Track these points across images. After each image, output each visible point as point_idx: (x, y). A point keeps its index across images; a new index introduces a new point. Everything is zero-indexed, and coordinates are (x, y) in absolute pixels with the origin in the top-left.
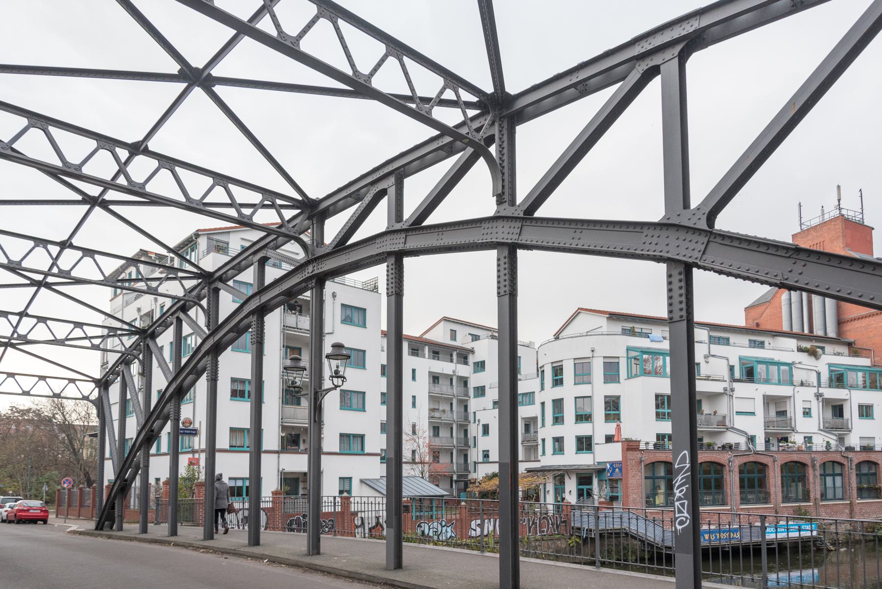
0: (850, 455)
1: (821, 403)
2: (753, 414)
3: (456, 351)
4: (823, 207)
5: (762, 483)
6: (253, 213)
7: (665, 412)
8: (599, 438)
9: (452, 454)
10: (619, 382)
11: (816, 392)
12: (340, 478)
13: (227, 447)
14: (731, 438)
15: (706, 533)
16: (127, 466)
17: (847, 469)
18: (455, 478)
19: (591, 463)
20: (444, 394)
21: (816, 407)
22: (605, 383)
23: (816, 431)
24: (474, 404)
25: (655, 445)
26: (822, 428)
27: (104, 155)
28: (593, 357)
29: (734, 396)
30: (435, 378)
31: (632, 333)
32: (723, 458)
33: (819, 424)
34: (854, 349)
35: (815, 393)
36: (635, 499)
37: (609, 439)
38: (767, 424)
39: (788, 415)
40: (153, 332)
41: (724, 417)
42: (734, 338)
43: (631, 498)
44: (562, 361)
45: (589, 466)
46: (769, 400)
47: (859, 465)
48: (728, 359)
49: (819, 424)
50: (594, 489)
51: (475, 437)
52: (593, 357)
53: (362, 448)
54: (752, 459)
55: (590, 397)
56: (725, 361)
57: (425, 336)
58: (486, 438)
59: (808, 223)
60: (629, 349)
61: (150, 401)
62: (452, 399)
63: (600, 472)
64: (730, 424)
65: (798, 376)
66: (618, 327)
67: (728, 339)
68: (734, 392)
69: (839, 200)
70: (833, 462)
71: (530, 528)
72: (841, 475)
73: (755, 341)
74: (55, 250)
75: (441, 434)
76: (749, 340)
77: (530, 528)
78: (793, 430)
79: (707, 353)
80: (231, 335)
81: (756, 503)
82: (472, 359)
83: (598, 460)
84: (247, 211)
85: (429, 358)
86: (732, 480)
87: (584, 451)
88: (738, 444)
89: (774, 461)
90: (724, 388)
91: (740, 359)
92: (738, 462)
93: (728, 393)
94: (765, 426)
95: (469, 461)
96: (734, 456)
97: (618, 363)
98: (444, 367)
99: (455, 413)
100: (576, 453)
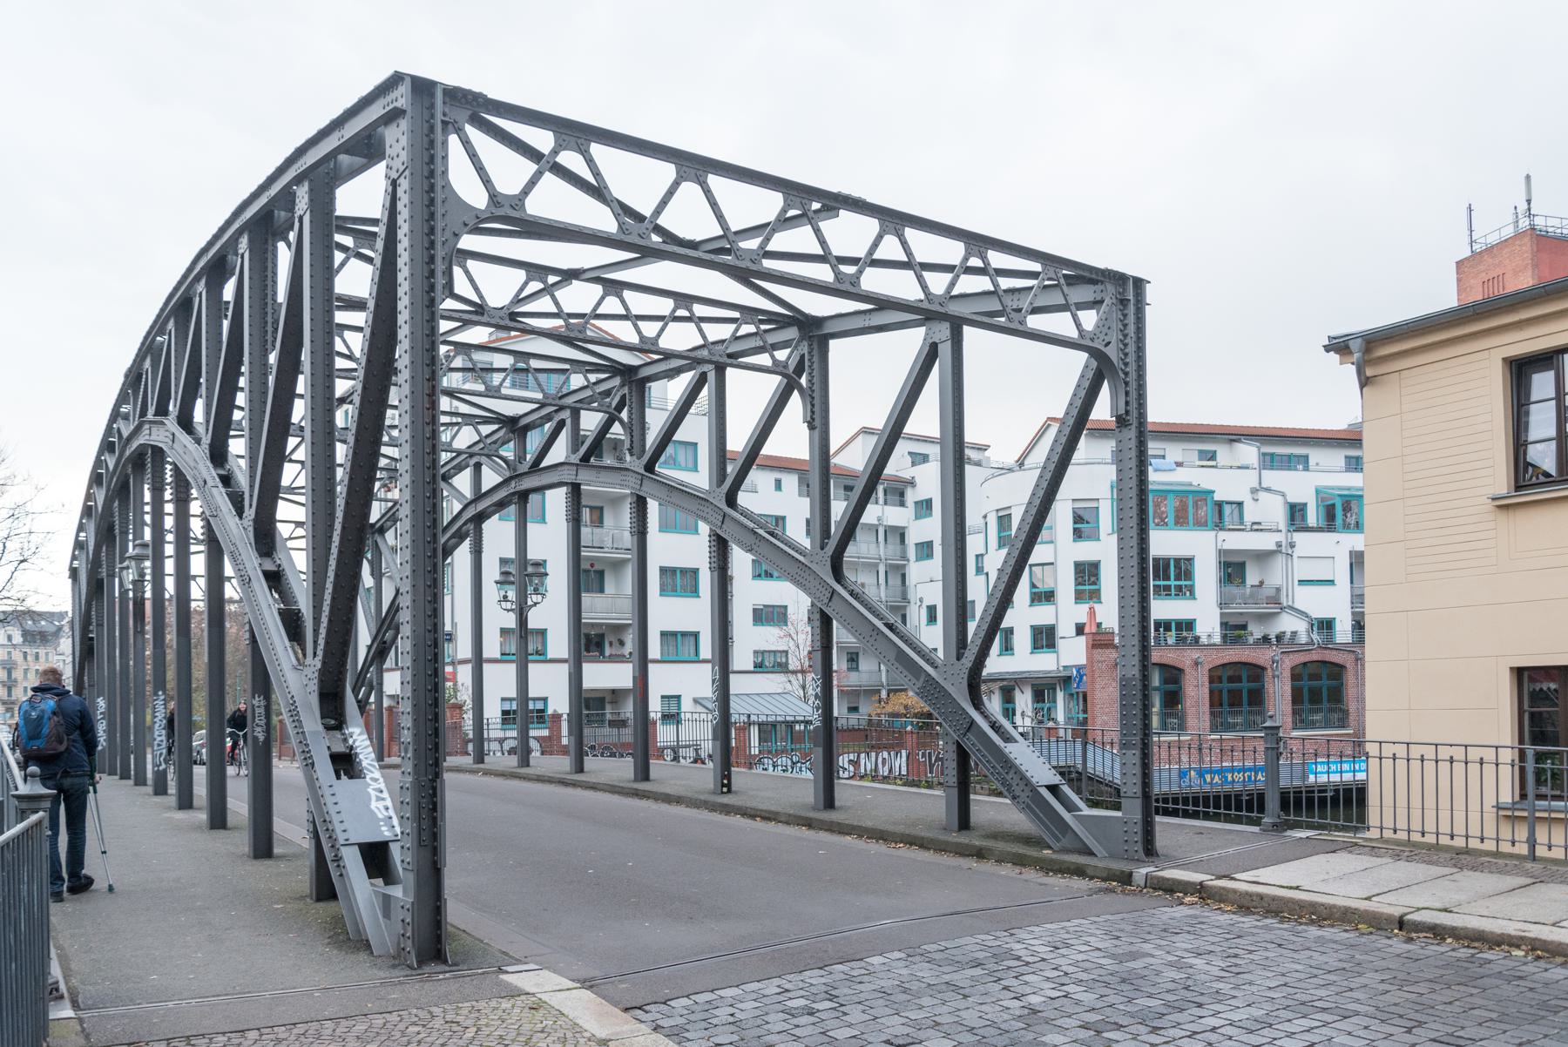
2: (1331, 582)
4: (1516, 208)
5: (1257, 698)
7: (1170, 586)
8: (1065, 629)
10: (1098, 539)
12: (663, 697)
13: (498, 655)
14: (1288, 624)
15: (1207, 773)
16: (359, 684)
19: (1054, 668)
20: (863, 558)
29: (1295, 555)
32: (1262, 656)
40: (382, 527)
41: (1278, 590)
42: (1316, 456)
45: (1049, 672)
48: (1284, 495)
53: (697, 653)
54: (1315, 656)
55: (1052, 564)
56: (1280, 498)
59: (1482, 240)
61: (381, 607)
62: (876, 565)
63: (1066, 680)
64: (1287, 601)
68: (1294, 549)
69: (1529, 201)
71: (931, 766)
76: (1346, 457)
77: (931, 766)
80: (454, 541)
81: (1325, 728)
82: (911, 496)
83: (1063, 663)
84: (975, 262)
87: (1045, 650)
88: (1294, 634)
90: (1277, 543)
91: (1318, 492)
92: (1288, 663)
94: (1352, 603)
100: (1031, 653)
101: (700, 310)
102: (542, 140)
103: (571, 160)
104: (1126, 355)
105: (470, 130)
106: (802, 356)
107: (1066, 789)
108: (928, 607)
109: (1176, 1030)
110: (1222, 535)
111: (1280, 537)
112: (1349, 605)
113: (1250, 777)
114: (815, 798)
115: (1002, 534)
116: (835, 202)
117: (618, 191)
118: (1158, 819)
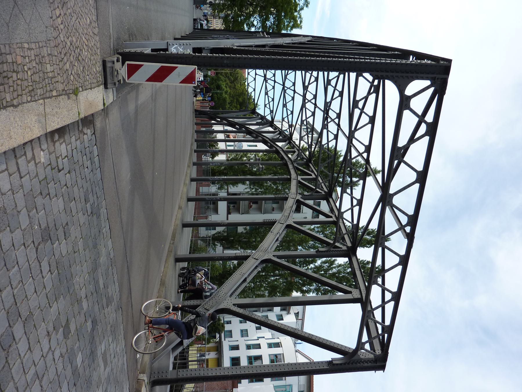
6: (379, 285)
27: (312, 97)
44: (282, 347)
74: (292, 88)
100: (230, 357)
101: (356, 209)
102: (430, 118)
103: (423, 128)
104: (356, 363)
105: (432, 89)
106: (341, 248)
107: (180, 349)
109: (47, 359)
114: (179, 255)
115: (272, 344)
116: (410, 238)
117: (413, 147)
118: (169, 386)
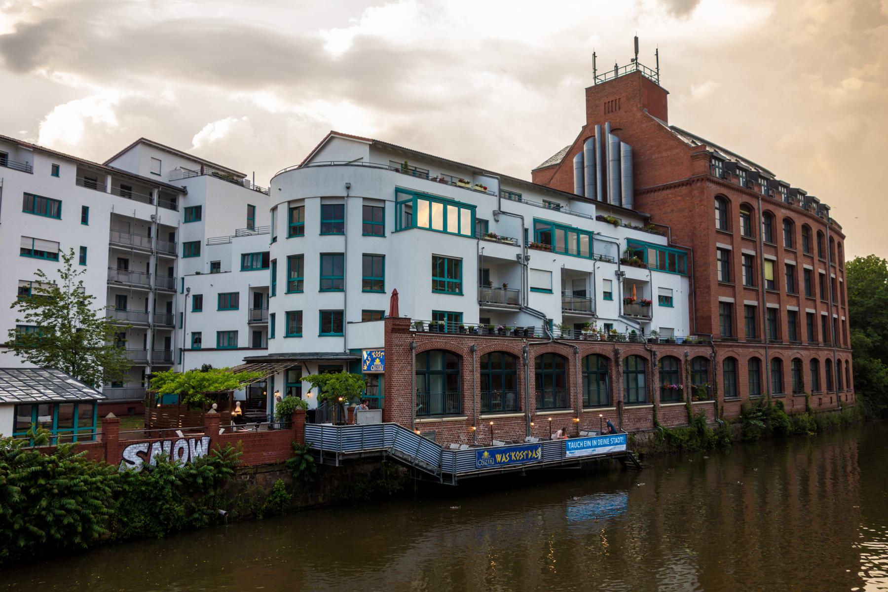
0: (655, 348)
1: (622, 284)
3: (158, 187)
5: (511, 383)
8: (353, 314)
9: (145, 336)
11: (617, 269)
14: (525, 321)
17: (650, 365)
18: (148, 371)
21: (616, 289)
22: (364, 235)
23: (617, 318)
24: (182, 266)
25: (430, 326)
26: (622, 314)
28: (348, 196)
30: (118, 221)
31: (405, 170)
32: (516, 346)
33: (620, 309)
34: (648, 225)
35: (616, 271)
36: (401, 405)
37: (369, 316)
38: (565, 307)
39: (588, 295)
43: (395, 403)
44: (303, 200)
46: (568, 275)
47: (662, 360)
48: (522, 218)
49: (620, 309)
50: (581, 373)
51: (182, 313)
52: (348, 196)
54: (549, 349)
57: (112, 165)
58: (197, 315)
59: (603, 78)
60: (398, 191)
62: (148, 257)
65: (599, 249)
66: (384, 161)
67: (520, 196)
70: (637, 356)
72: (643, 372)
73: (549, 203)
75: (128, 308)
78: (593, 315)
79: (496, 208)
82: (182, 203)
83: (352, 345)
85: (113, 193)
86: (528, 376)
89: (575, 353)
93: (521, 262)
94: (563, 309)
95: (172, 348)
96: (530, 344)
97: (383, 209)
98: (141, 210)
99: (152, 278)
108: (194, 296)
110: (482, 244)
111: (517, 251)
112: (560, 310)
113: (527, 455)
